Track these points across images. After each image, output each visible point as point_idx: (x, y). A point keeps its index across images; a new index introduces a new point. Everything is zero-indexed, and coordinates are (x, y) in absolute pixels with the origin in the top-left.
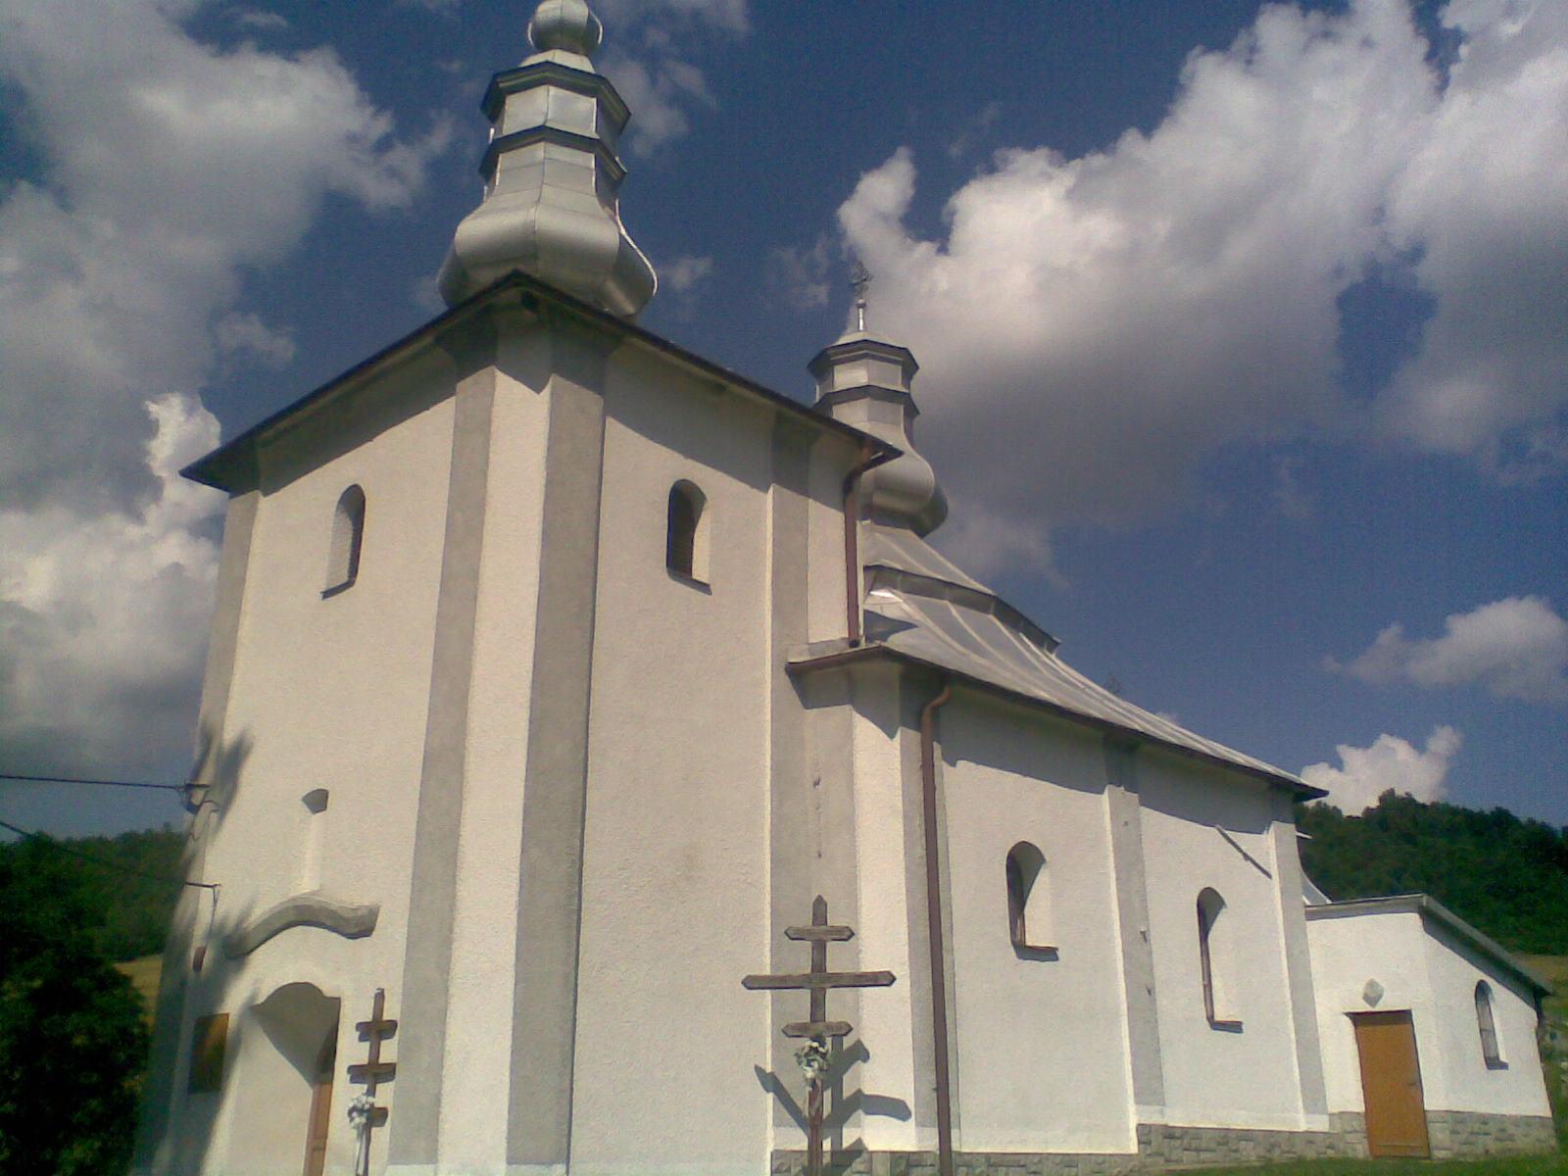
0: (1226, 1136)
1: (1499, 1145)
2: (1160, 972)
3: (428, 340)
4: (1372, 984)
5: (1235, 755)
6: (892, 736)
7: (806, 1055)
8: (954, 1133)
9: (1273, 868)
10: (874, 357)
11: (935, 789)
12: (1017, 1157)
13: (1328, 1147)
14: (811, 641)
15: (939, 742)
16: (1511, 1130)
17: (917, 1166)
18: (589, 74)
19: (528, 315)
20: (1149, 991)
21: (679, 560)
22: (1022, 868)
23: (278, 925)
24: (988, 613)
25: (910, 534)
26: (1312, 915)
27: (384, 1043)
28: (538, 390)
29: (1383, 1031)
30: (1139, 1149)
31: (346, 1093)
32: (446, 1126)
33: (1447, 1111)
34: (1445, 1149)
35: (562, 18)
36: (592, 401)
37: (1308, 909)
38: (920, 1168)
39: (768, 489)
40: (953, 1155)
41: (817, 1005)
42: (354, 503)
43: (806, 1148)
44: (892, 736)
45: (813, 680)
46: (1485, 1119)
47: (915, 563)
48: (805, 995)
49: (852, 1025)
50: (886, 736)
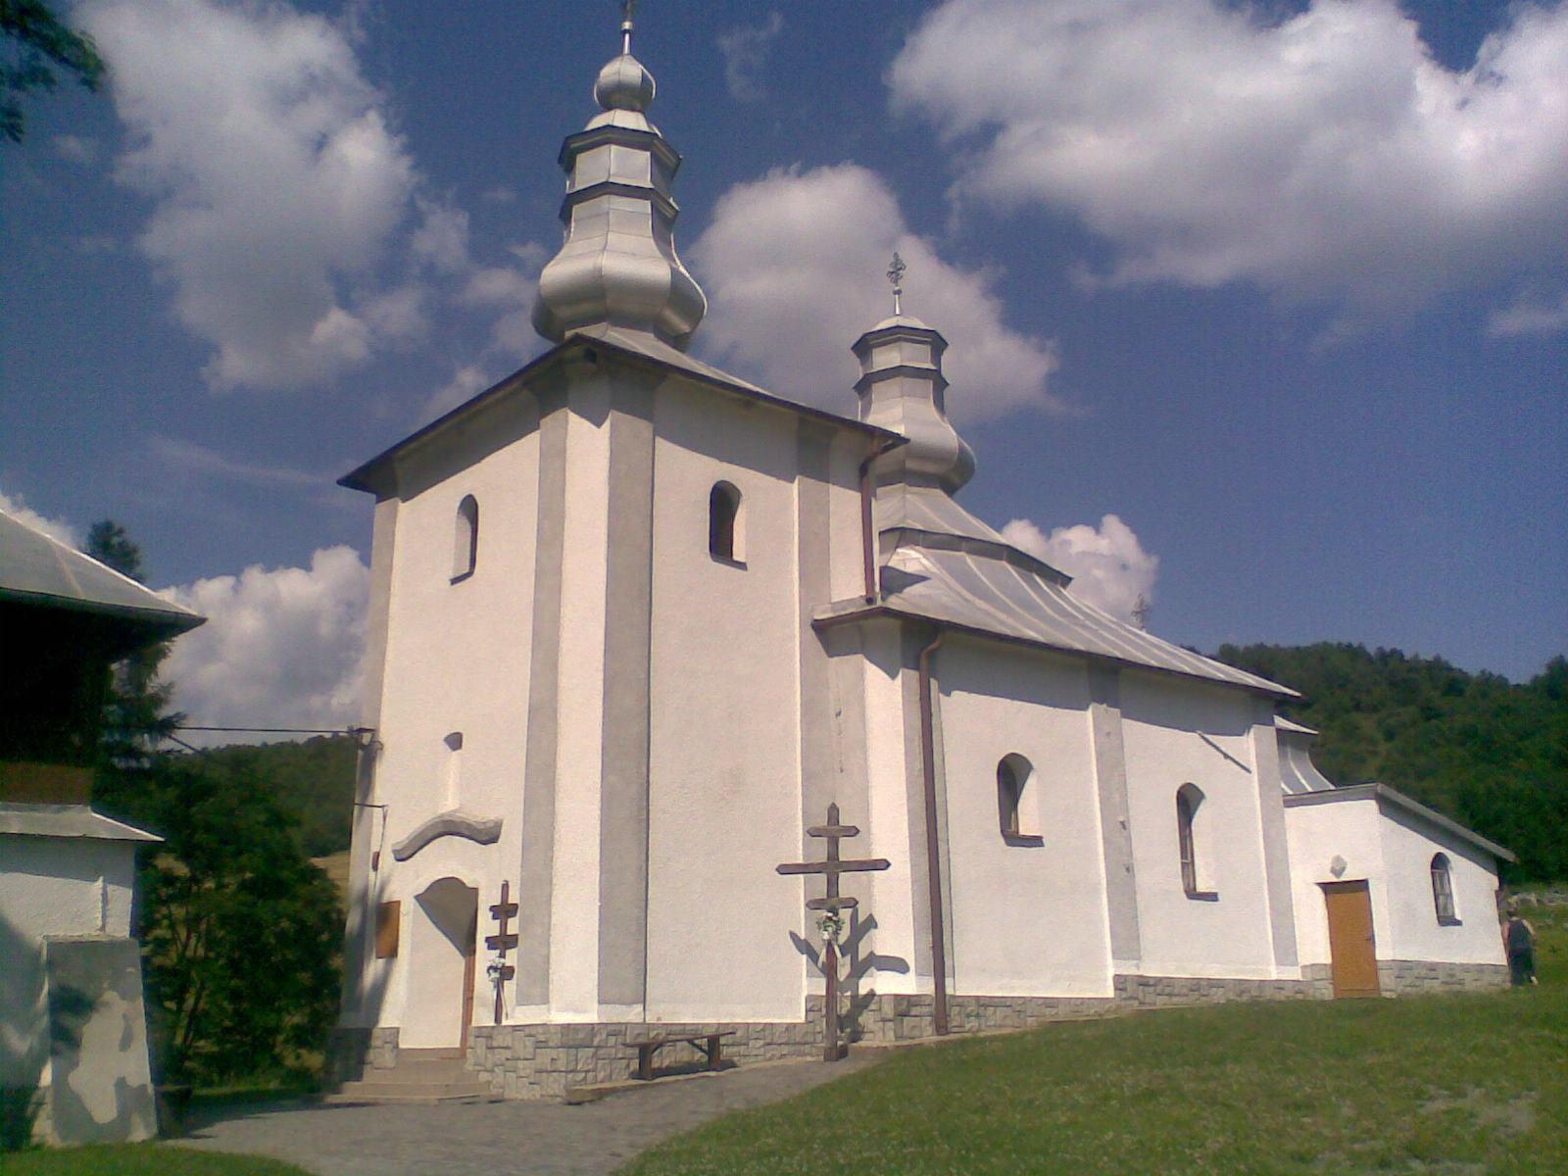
0: (1198, 983)
1: (1447, 988)
2: (1139, 852)
3: (516, 385)
4: (1338, 859)
5: (1219, 670)
6: (893, 676)
7: (824, 922)
8: (948, 981)
9: (1254, 768)
10: (906, 340)
11: (931, 715)
12: (1003, 1000)
13: (1297, 993)
14: (833, 601)
15: (936, 678)
16: (1460, 975)
17: (917, 1005)
18: (645, 132)
19: (592, 366)
20: (1128, 870)
21: (720, 544)
22: (1011, 775)
23: (430, 835)
24: (1001, 559)
25: (939, 493)
26: (1290, 802)
27: (510, 921)
28: (599, 425)
29: (1346, 897)
30: (1115, 994)
31: (485, 956)
32: (553, 977)
33: (1393, 961)
34: (1391, 990)
35: (620, 82)
36: (644, 427)
37: (1288, 798)
38: (919, 1008)
39: (794, 479)
40: (947, 998)
41: (833, 884)
42: (470, 508)
43: (824, 993)
44: (893, 676)
45: (834, 634)
46: (1432, 967)
47: (938, 520)
48: (823, 877)
49: (857, 899)
50: (886, 676)
